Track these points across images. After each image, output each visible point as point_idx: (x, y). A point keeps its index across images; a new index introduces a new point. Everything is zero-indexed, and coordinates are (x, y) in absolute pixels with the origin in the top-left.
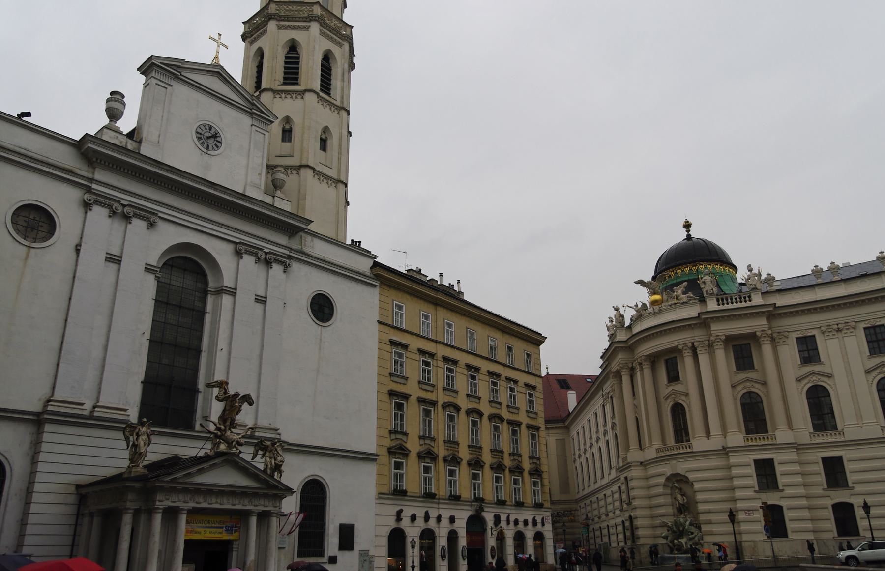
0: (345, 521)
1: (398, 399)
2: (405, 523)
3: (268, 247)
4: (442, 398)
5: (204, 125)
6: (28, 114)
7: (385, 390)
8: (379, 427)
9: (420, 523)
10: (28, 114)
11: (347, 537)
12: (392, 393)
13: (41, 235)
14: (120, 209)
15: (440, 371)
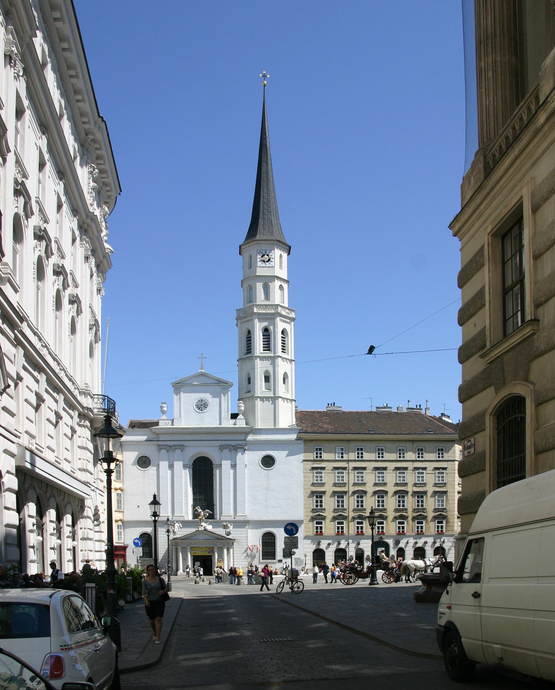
2: (323, 546)
3: (233, 443)
7: (309, 492)
8: (305, 508)
9: (333, 548)
12: (313, 493)
15: (351, 475)
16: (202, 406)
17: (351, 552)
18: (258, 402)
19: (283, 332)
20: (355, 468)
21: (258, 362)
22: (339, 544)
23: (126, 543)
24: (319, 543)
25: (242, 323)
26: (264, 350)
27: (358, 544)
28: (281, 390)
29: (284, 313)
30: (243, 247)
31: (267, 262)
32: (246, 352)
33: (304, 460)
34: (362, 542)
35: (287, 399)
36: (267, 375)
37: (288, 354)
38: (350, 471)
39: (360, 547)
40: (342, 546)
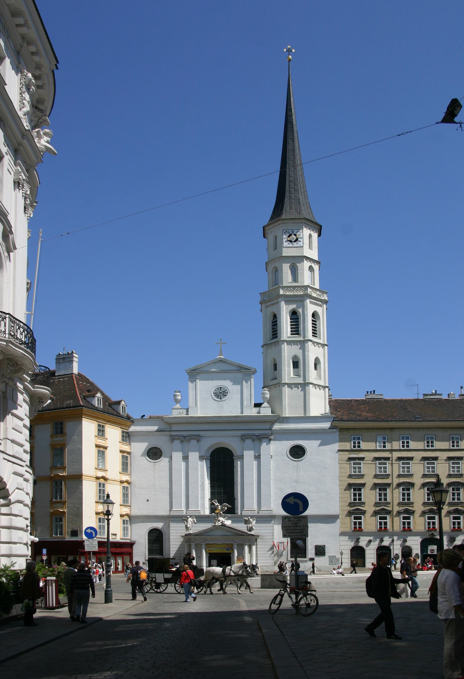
0: (320, 543)
1: (357, 488)
2: (363, 542)
3: (257, 433)
4: (396, 481)
5: (225, 395)
6: (144, 416)
9: (375, 544)
10: (144, 416)
11: (320, 551)
13: (158, 457)
14: (256, 437)
15: (396, 467)
16: (221, 394)
17: (397, 550)
18: (286, 390)
19: (314, 315)
20: (400, 459)
21: (285, 347)
22: (382, 541)
23: (133, 539)
24: (358, 540)
25: (266, 307)
26: (292, 334)
27: (405, 541)
28: (312, 376)
29: (314, 295)
30: (267, 228)
31: (294, 242)
32: (271, 336)
33: (340, 451)
34: (409, 538)
35: (319, 386)
36: (296, 360)
37: (320, 338)
38: (394, 462)
39: (407, 544)
40: (386, 543)
